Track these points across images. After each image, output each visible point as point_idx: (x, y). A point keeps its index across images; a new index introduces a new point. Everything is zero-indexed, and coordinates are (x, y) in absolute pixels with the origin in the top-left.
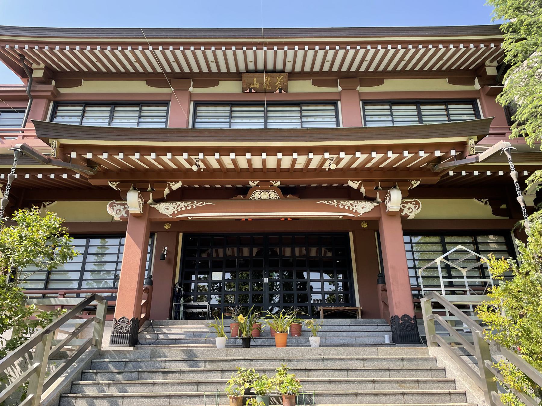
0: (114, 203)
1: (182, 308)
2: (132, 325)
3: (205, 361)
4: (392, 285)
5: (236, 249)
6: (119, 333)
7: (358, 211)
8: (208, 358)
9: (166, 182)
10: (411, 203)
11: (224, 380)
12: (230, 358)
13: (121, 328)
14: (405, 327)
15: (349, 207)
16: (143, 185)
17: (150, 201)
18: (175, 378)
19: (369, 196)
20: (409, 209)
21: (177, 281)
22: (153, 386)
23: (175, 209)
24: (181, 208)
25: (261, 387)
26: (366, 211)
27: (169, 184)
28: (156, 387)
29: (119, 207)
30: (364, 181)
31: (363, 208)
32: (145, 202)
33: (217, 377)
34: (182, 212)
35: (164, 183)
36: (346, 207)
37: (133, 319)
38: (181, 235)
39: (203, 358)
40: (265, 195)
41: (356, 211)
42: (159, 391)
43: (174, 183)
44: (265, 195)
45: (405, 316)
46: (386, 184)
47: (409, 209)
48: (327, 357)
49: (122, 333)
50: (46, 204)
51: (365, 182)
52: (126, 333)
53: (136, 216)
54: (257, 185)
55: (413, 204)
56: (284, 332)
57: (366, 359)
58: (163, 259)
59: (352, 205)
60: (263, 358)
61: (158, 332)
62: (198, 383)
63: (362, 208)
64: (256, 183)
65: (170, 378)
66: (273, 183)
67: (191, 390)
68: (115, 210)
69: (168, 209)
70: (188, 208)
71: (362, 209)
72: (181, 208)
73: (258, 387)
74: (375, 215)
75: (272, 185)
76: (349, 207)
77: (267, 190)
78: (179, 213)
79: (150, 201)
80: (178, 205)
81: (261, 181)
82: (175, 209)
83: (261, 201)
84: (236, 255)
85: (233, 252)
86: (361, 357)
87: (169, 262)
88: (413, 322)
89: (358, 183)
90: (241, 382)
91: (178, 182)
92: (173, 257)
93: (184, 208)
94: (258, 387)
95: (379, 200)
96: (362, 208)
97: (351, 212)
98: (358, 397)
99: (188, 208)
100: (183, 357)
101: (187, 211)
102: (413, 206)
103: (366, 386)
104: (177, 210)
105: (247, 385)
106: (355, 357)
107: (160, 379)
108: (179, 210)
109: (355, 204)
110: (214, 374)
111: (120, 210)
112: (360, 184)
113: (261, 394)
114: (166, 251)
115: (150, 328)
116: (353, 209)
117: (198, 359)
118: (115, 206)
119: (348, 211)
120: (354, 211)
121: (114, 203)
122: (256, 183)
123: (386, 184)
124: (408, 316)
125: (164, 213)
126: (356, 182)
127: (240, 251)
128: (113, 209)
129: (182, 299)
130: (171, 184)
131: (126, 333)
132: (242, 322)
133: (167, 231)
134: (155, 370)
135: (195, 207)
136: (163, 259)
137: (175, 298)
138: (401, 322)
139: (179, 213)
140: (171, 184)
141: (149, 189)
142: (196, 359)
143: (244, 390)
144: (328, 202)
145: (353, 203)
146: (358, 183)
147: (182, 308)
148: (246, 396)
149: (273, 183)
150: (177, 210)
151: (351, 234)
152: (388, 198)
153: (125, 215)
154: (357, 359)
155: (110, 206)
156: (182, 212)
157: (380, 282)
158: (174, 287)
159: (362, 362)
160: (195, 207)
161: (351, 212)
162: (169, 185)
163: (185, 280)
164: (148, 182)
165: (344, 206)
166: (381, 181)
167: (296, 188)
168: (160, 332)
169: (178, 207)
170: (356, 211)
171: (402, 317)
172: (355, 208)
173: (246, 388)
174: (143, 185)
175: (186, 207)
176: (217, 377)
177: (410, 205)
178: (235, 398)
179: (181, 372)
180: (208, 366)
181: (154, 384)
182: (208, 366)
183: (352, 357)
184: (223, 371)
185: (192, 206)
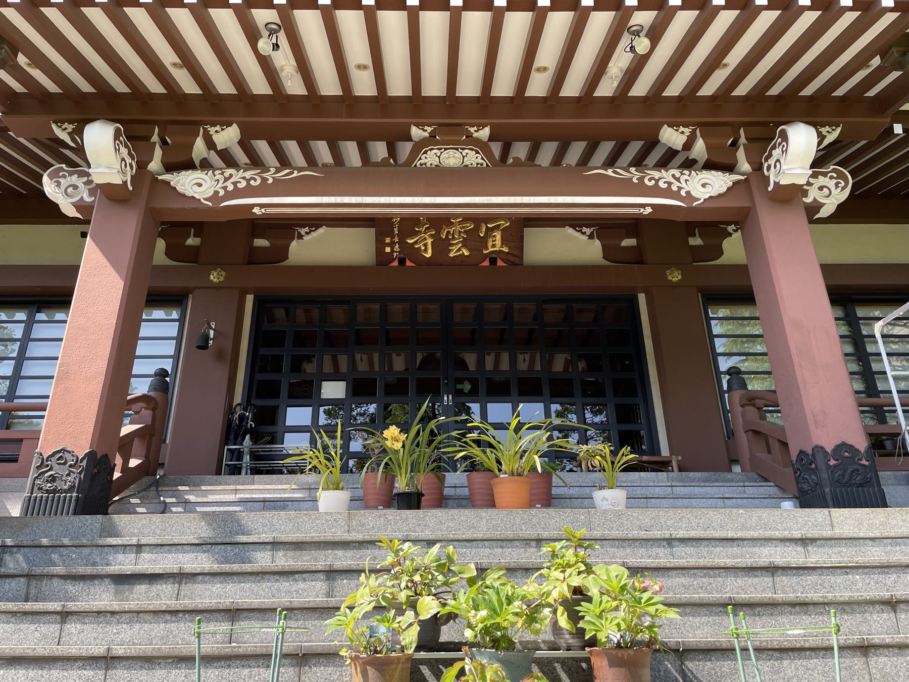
0: (62, 169)
1: (247, 458)
2: (87, 470)
3: (275, 545)
4: (797, 368)
5: (376, 356)
6: (48, 492)
7: (694, 194)
8: (283, 538)
9: (199, 123)
10: (825, 175)
11: (332, 602)
12: (360, 537)
13: (53, 479)
14: (847, 476)
15: (670, 184)
16: (139, 130)
17: (155, 165)
18: (163, 596)
19: (718, 159)
20: (821, 188)
21: (238, 398)
22: (63, 621)
23: (220, 185)
24: (235, 184)
25: (494, 612)
26: (714, 193)
27: (205, 130)
28: (72, 627)
29: (74, 179)
30: (700, 125)
31: (706, 186)
32: (142, 166)
33: (312, 592)
34: (237, 193)
35: (192, 127)
36: (662, 185)
37: (91, 455)
38: (250, 299)
39: (264, 537)
40: (451, 158)
41: (688, 193)
42: (83, 638)
43: (218, 128)
44: (451, 158)
45: (843, 447)
46: (757, 132)
47: (821, 188)
48: (681, 534)
49: (55, 491)
50: (303, 231)
51: (707, 128)
52: (66, 491)
53: (112, 194)
54: (432, 136)
55: (831, 177)
56: (519, 475)
57: (813, 540)
58: (204, 347)
59: (678, 180)
60: (468, 536)
61: (168, 500)
62: (233, 613)
63: (704, 185)
64: (429, 129)
65: (141, 596)
66: (472, 130)
67: (215, 636)
68: (63, 187)
69: (200, 185)
70: (252, 182)
71: (702, 189)
72: (235, 184)
73: (484, 613)
74: (739, 202)
75: (469, 136)
76: (670, 184)
77: (456, 144)
78: (229, 195)
79: (155, 165)
80: (227, 174)
81: (440, 125)
82: (220, 185)
83: (439, 171)
84: (377, 369)
85: (371, 362)
86: (797, 534)
87: (220, 355)
88: (864, 462)
89: (687, 131)
90: (403, 596)
91: (229, 125)
92: (228, 345)
93: (243, 184)
94: (484, 613)
95: (745, 167)
96: (704, 185)
97: (676, 195)
98: (873, 660)
99: (252, 182)
100: (204, 531)
101: (250, 191)
102: (831, 184)
103: (865, 621)
104: (225, 188)
105: (429, 607)
106: (778, 534)
107: (103, 597)
108: (231, 188)
109: (686, 177)
110: (301, 585)
111: (75, 187)
112: (693, 133)
113: (496, 643)
114: (212, 333)
115: (152, 492)
116: (680, 188)
117: (251, 539)
118: (64, 176)
119: (668, 193)
120: (683, 193)
121: (62, 169)
122: (429, 129)
123: (757, 132)
124: (851, 446)
125: (189, 193)
126: (682, 129)
127: (387, 360)
128: (59, 184)
129: (248, 437)
130: (212, 130)
131: (66, 491)
132: (398, 446)
133: (217, 287)
134: (89, 570)
135: (270, 181)
136: (204, 347)
137: (232, 437)
138: (832, 462)
139: (229, 195)
140: (212, 130)
141: (155, 138)
142: (243, 539)
143: (416, 629)
144: (614, 172)
145: (678, 175)
146: (687, 131)
147: (247, 458)
148: (423, 655)
149: (472, 130)
150: (225, 188)
151: (642, 298)
152: (776, 153)
153: (88, 199)
154: (783, 540)
155: (51, 177)
156: (237, 193)
157: (735, 386)
158: (230, 410)
159: (800, 549)
160: (270, 181)
161: (676, 195)
162: (206, 132)
163: (257, 397)
164: (153, 123)
165: (657, 181)
166: (745, 125)
167: (533, 127)
168: (174, 500)
169: (226, 179)
170: (688, 193)
171: (834, 450)
172: (684, 185)
173: (425, 616)
174: (139, 130)
175: (248, 181)
176: (312, 592)
177: (822, 181)
178: (376, 659)
179: (181, 577)
180: (283, 560)
181: (65, 616)
182: (283, 560)
183: (768, 534)
184: (331, 574)
185: (264, 180)
